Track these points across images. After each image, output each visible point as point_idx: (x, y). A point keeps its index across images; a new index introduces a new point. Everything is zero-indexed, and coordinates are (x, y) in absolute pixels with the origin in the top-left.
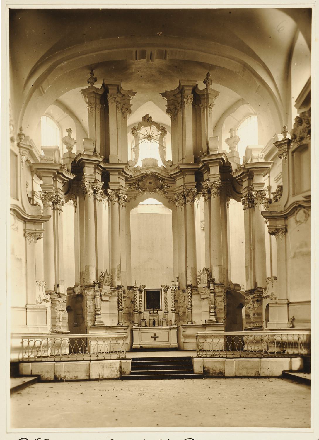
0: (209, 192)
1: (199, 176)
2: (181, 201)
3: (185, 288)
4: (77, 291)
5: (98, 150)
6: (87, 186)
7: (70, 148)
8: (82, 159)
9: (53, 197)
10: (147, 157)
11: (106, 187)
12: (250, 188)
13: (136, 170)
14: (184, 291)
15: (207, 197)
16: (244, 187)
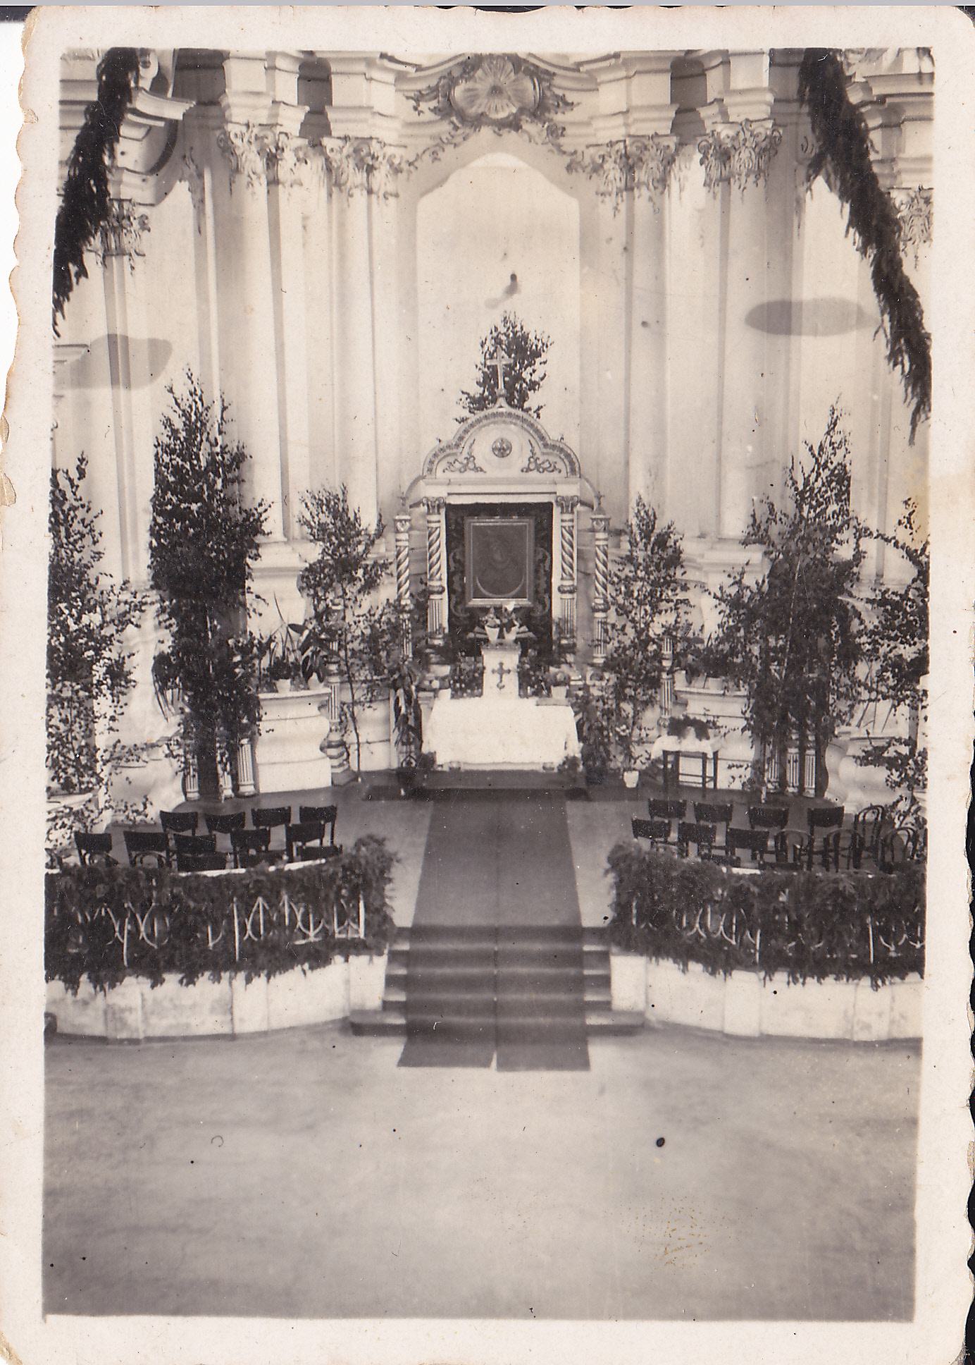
0: (725, 156)
6: (237, 142)
11: (316, 127)
15: (715, 174)
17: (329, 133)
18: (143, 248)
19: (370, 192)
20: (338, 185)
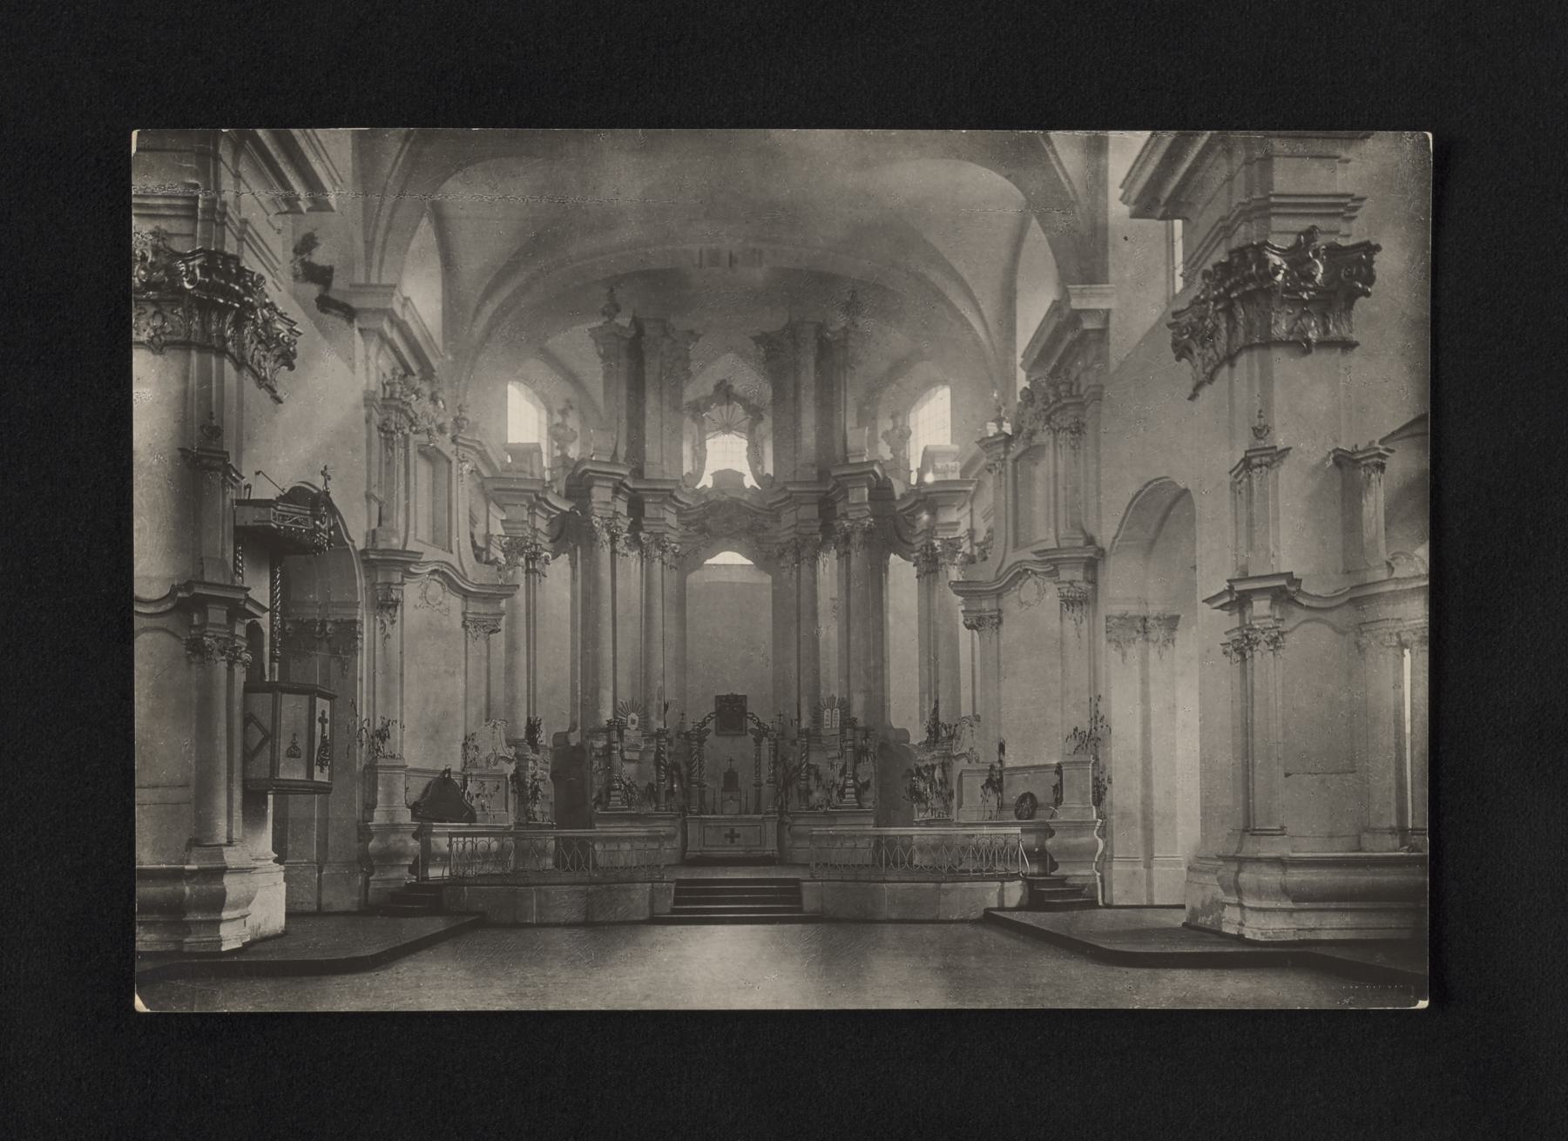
0: (847, 539)
1: (827, 507)
2: (790, 557)
5: (622, 450)
8: (586, 471)
10: (722, 467)
12: (930, 531)
13: (699, 494)
14: (794, 743)
17: (642, 529)
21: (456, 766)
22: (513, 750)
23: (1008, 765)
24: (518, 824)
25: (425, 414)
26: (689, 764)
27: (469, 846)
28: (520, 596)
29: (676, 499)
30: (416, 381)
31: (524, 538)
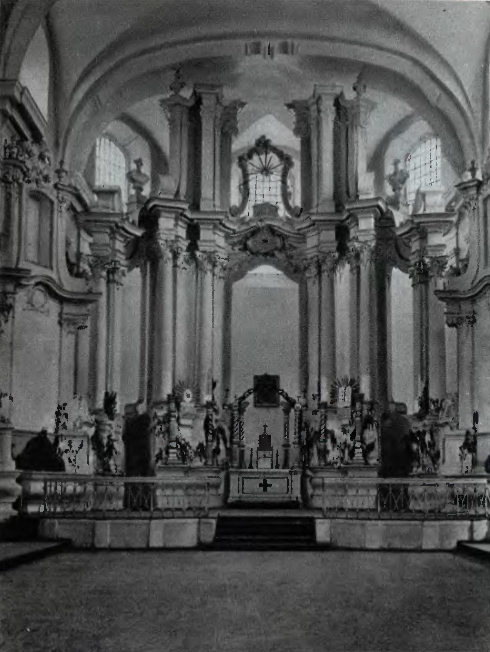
0: (357, 256)
3: (316, 407)
4: (142, 409)
5: (183, 190)
7: (139, 189)
8: (155, 206)
9: (108, 264)
12: (422, 252)
14: (315, 413)
15: (354, 265)
16: (413, 250)
17: (198, 249)
18: (123, 282)
19: (214, 275)
20: (201, 269)
21: (51, 430)
22: (93, 417)
23: (480, 430)
24: (97, 473)
25: (35, 168)
26: (231, 428)
27: (59, 488)
28: (103, 300)
29: (224, 226)
30: (29, 144)
31: (107, 257)
